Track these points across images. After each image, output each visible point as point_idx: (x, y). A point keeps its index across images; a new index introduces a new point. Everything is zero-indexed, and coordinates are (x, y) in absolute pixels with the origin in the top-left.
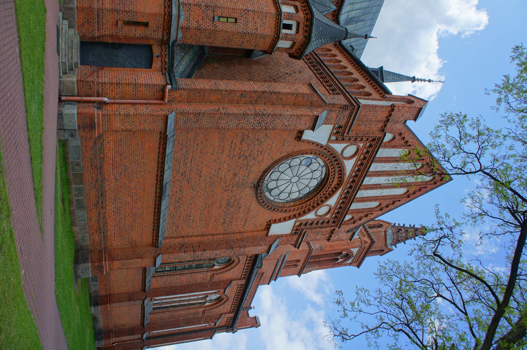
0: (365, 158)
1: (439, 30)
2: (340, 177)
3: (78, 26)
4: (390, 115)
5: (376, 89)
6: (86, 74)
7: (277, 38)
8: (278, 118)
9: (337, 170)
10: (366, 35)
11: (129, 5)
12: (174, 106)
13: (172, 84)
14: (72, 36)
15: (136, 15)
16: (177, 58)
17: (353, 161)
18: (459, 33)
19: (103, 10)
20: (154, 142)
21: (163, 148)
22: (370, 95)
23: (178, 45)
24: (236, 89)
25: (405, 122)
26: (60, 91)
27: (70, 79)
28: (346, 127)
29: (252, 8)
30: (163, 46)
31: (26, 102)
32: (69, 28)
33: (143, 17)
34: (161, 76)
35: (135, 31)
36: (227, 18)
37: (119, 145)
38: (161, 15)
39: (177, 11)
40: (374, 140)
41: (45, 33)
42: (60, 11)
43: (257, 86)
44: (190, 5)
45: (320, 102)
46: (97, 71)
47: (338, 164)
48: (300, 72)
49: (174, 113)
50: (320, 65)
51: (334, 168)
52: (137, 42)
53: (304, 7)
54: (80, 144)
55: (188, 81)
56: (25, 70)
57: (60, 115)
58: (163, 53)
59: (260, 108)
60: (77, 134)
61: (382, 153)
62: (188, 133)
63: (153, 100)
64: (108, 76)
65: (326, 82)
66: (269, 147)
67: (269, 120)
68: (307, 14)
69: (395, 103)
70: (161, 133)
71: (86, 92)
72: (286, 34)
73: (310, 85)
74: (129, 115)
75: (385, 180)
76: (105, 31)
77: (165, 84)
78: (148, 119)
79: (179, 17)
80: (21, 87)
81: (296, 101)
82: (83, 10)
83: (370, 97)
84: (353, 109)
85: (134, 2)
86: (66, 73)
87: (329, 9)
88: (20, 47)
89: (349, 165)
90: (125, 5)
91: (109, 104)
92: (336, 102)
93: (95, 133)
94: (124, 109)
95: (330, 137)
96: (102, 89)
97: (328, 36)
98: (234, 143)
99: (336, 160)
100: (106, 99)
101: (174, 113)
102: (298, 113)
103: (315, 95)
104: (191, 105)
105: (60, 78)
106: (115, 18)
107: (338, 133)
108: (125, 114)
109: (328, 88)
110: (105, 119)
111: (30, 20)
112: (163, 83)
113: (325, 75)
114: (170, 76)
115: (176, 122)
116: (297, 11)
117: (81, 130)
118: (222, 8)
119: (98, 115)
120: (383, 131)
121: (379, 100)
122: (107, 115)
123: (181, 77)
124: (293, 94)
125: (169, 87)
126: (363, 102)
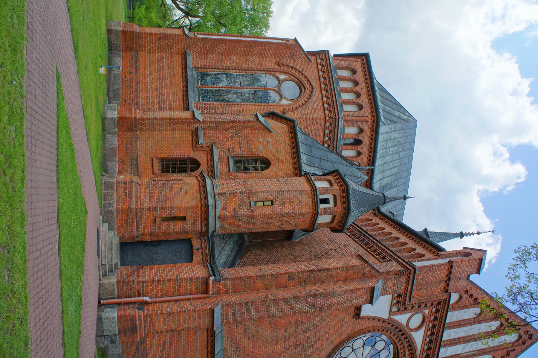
0: (434, 326)
1: (478, 191)
2: (412, 354)
3: (118, 228)
4: (450, 273)
5: (427, 248)
6: (126, 274)
7: (316, 214)
8: (331, 296)
9: (406, 345)
10: (405, 196)
11: (166, 201)
12: (219, 298)
13: (215, 276)
14: (112, 238)
15: (174, 210)
16: (218, 249)
17: (422, 331)
18: (501, 190)
19: (141, 209)
20: (201, 340)
21: (212, 347)
22: (423, 255)
23: (218, 236)
24: (282, 271)
25: (469, 277)
26: (99, 294)
27: (110, 281)
28: (406, 294)
29: (286, 189)
30: (202, 238)
31: (62, 302)
32: (109, 230)
33: (180, 211)
34: (203, 269)
35: (174, 226)
36: (264, 202)
37: (163, 348)
38: (198, 207)
39: (213, 201)
40: (439, 303)
41: (85, 233)
42: (101, 214)
43: (303, 266)
44: (225, 194)
45: (373, 272)
46: (138, 270)
47: (406, 338)
48: (345, 246)
49: (220, 306)
50: (364, 235)
51: (402, 344)
52: (175, 237)
53: (337, 179)
54: (121, 352)
55: (232, 270)
56: (63, 267)
57: (100, 320)
58: (203, 246)
59: (310, 289)
60: (118, 339)
61: (452, 316)
62: (237, 327)
63: (197, 294)
64: (148, 274)
65: (375, 251)
66: (327, 330)
67: (322, 300)
68: (342, 186)
69: (451, 259)
70: (207, 330)
71: (126, 293)
72: (325, 209)
73: (359, 256)
74: (173, 313)
75: (464, 348)
76: (144, 230)
77: (208, 276)
78: (193, 315)
79: (215, 206)
80: (58, 284)
81: (347, 275)
82: (122, 211)
83: (424, 258)
84: (410, 273)
85: (171, 198)
86: (106, 275)
87: (361, 179)
88: (60, 243)
89: (418, 337)
90: (162, 202)
91: (150, 303)
92: (389, 269)
93: (137, 336)
94: (167, 307)
95: (391, 309)
96: (143, 288)
97: (367, 204)
98: (288, 332)
99: (403, 334)
100: (147, 299)
101: (220, 306)
102: (352, 288)
103: (366, 265)
104: (237, 295)
105: (100, 280)
106: (153, 216)
107: (398, 302)
108: (168, 313)
109: (377, 257)
110: (147, 320)
111: (71, 220)
112: (206, 275)
113: (371, 244)
114: (212, 267)
115: (223, 315)
116: (331, 185)
117: (122, 335)
118: (257, 192)
119: (140, 316)
120: (447, 291)
121: (434, 259)
122: (149, 315)
123: (224, 267)
124: (343, 268)
125: (212, 278)
126: (417, 264)
